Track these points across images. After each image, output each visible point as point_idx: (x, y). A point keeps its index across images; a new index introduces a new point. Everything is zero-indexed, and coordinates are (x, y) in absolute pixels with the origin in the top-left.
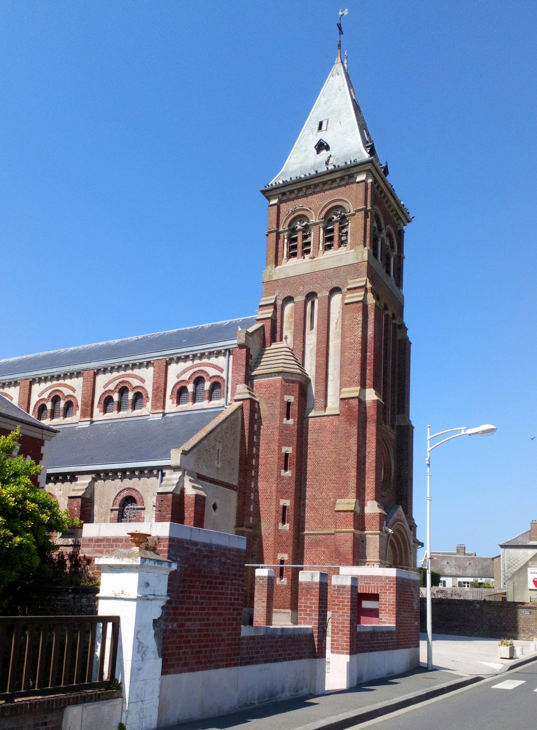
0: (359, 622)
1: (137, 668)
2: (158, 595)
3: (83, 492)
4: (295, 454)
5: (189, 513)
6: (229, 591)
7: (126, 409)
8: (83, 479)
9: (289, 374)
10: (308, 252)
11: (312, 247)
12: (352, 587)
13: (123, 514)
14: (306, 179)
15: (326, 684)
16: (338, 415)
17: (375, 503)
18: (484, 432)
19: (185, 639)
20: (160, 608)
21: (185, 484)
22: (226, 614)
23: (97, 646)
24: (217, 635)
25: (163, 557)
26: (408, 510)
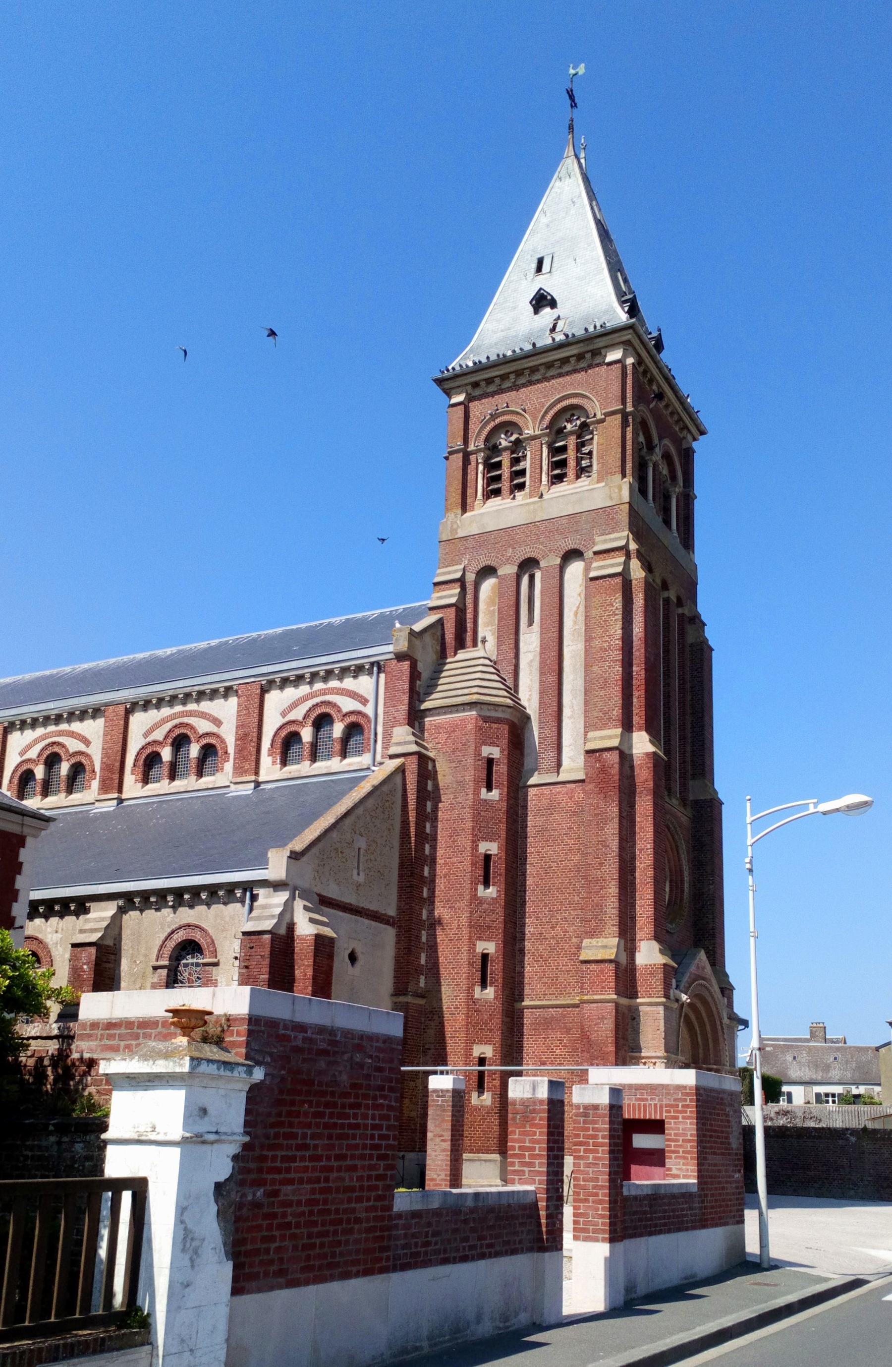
0: (628, 1178)
1: (182, 1283)
2: (225, 1134)
3: (100, 935)
4: (503, 855)
5: (304, 970)
6: (370, 1122)
7: (185, 775)
8: (102, 910)
9: (490, 707)
10: (521, 487)
11: (527, 479)
12: (612, 1107)
13: (176, 975)
14: (515, 359)
15: (564, 1303)
16: (583, 781)
17: (655, 946)
18: (850, 808)
19: (280, 1220)
20: (229, 1160)
21: (295, 915)
22: (363, 1167)
23: (102, 1237)
24: (345, 1211)
25: (237, 1055)
26: (716, 958)
